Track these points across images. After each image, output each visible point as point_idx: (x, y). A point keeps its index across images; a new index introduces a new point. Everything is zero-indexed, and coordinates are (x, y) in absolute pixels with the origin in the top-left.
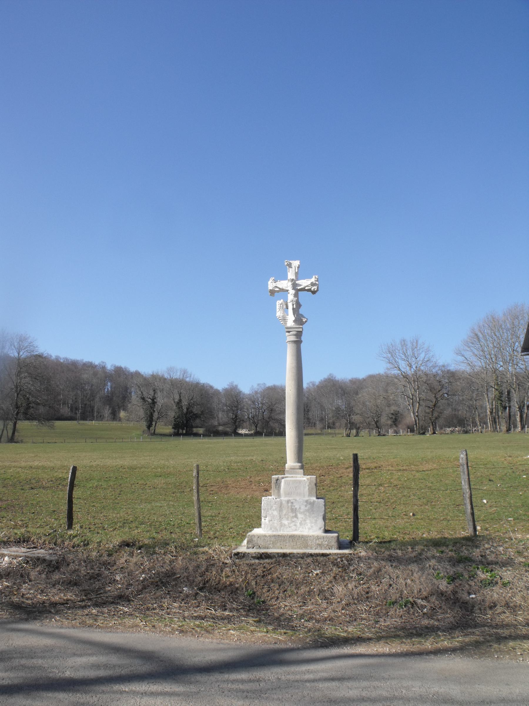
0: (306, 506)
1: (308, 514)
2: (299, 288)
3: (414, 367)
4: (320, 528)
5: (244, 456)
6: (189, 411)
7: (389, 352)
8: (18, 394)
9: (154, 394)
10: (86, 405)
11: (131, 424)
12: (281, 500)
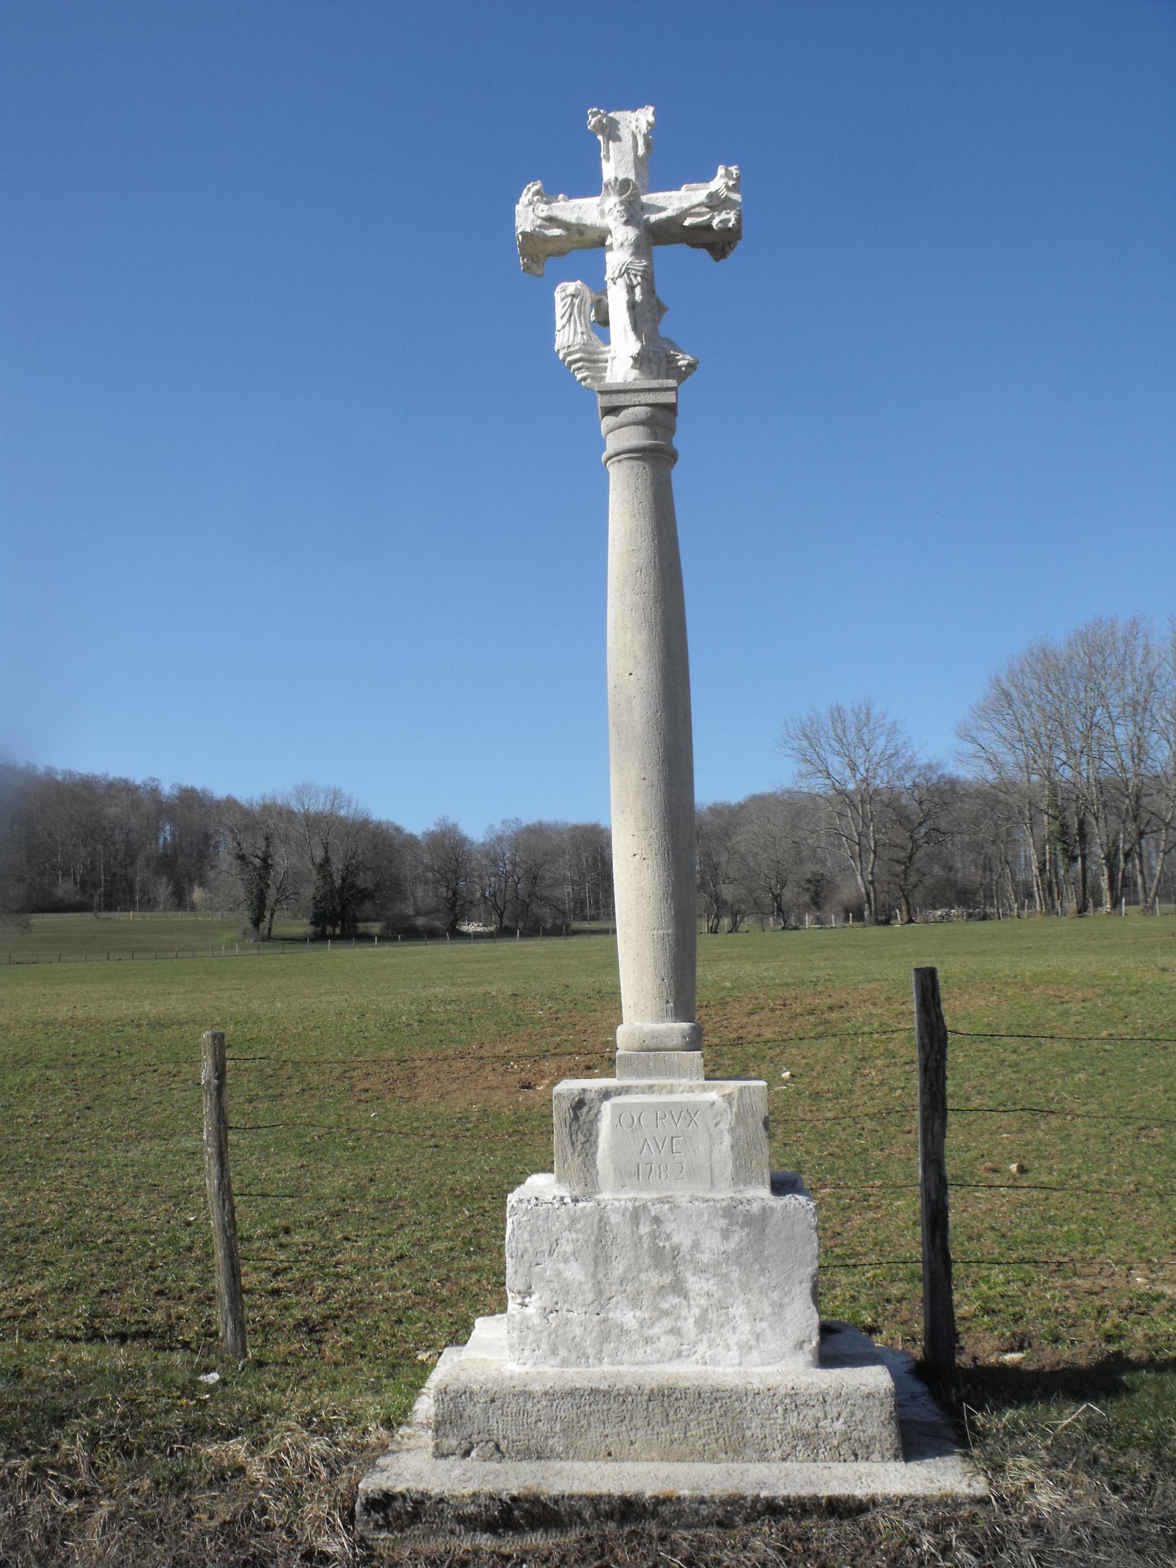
0: (726, 1234)
1: (735, 1275)
2: (654, 218)
3: (862, 769)
4: (800, 1345)
5: (470, 984)
7: (805, 735)
9: (268, 846)
10: (115, 875)
11: (217, 917)
12: (601, 1208)
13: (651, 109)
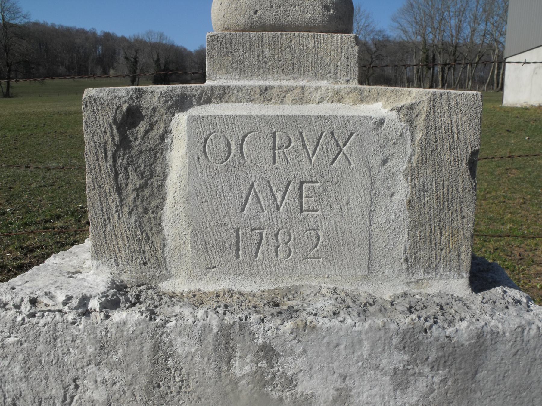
6: (166, 69)
8: (7, 54)
10: (81, 65)
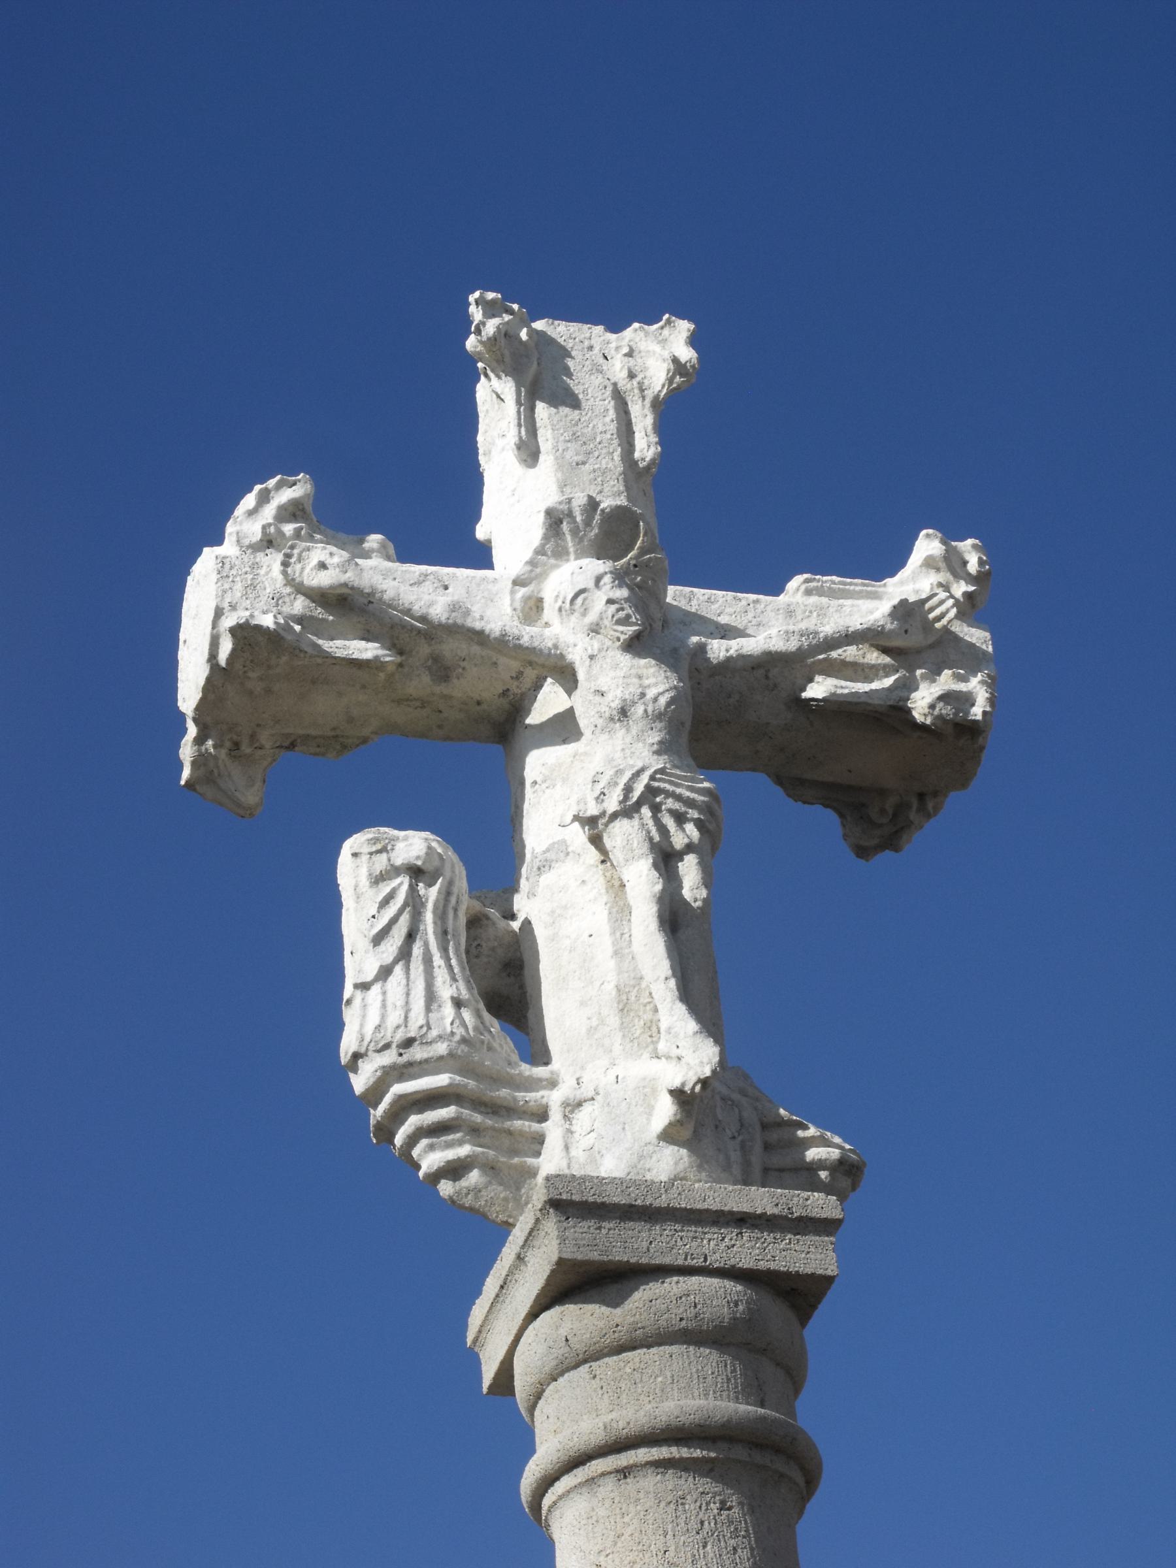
2: (718, 650)
13: (684, 327)
